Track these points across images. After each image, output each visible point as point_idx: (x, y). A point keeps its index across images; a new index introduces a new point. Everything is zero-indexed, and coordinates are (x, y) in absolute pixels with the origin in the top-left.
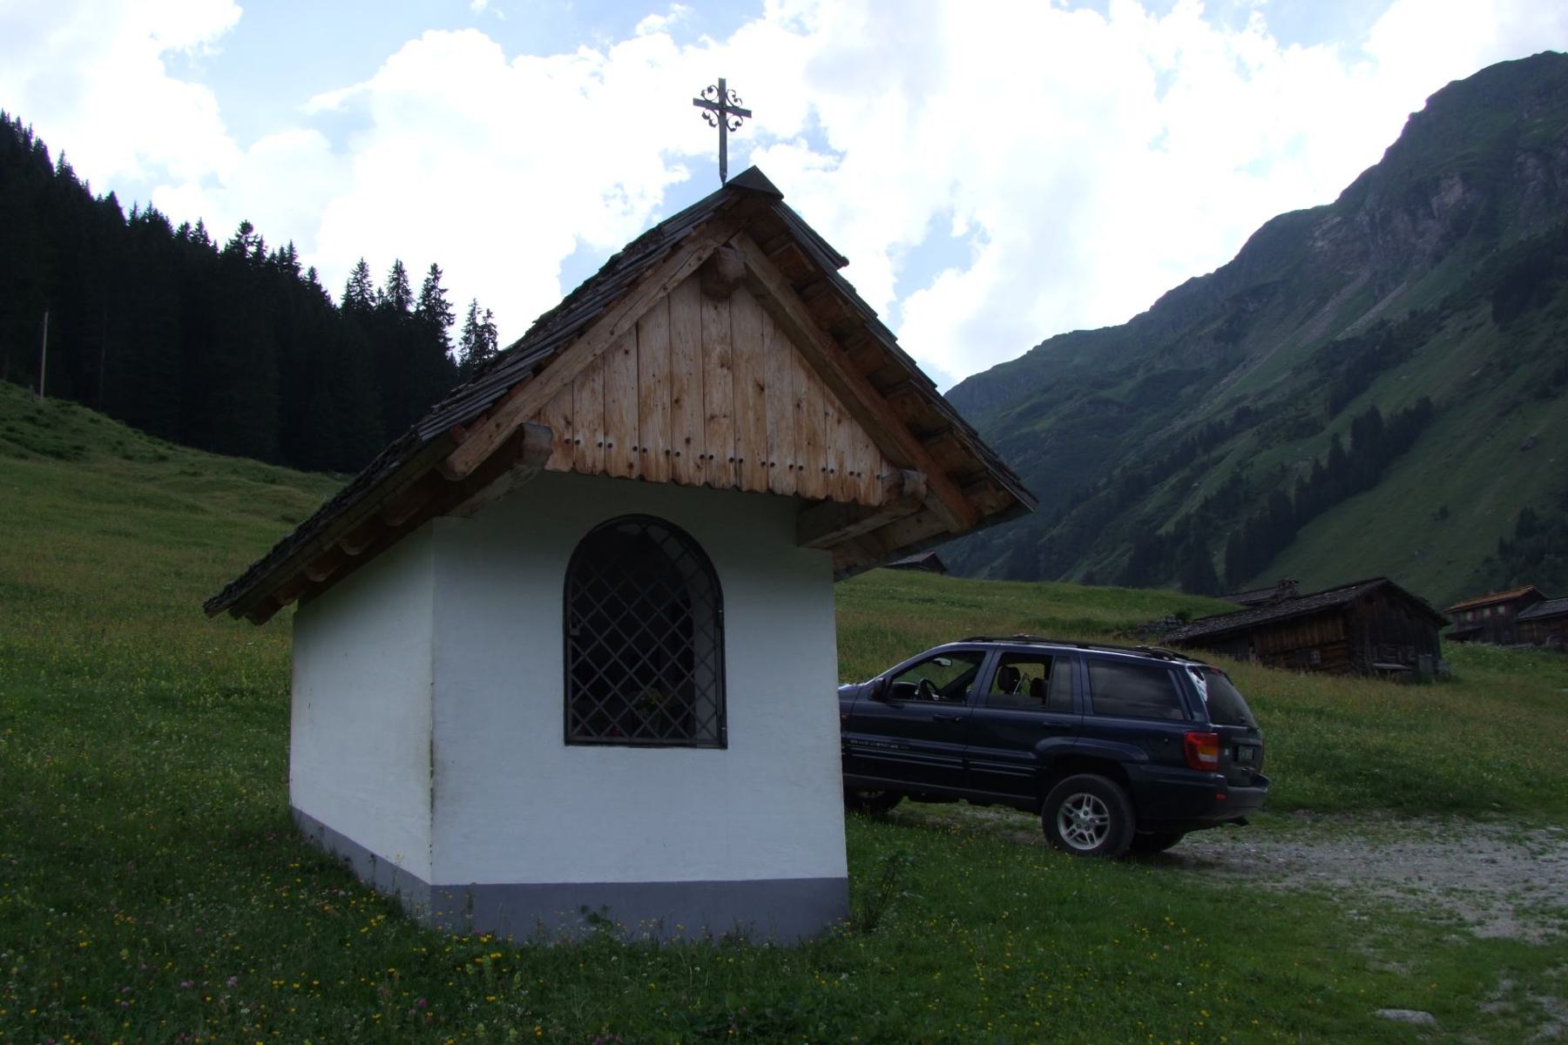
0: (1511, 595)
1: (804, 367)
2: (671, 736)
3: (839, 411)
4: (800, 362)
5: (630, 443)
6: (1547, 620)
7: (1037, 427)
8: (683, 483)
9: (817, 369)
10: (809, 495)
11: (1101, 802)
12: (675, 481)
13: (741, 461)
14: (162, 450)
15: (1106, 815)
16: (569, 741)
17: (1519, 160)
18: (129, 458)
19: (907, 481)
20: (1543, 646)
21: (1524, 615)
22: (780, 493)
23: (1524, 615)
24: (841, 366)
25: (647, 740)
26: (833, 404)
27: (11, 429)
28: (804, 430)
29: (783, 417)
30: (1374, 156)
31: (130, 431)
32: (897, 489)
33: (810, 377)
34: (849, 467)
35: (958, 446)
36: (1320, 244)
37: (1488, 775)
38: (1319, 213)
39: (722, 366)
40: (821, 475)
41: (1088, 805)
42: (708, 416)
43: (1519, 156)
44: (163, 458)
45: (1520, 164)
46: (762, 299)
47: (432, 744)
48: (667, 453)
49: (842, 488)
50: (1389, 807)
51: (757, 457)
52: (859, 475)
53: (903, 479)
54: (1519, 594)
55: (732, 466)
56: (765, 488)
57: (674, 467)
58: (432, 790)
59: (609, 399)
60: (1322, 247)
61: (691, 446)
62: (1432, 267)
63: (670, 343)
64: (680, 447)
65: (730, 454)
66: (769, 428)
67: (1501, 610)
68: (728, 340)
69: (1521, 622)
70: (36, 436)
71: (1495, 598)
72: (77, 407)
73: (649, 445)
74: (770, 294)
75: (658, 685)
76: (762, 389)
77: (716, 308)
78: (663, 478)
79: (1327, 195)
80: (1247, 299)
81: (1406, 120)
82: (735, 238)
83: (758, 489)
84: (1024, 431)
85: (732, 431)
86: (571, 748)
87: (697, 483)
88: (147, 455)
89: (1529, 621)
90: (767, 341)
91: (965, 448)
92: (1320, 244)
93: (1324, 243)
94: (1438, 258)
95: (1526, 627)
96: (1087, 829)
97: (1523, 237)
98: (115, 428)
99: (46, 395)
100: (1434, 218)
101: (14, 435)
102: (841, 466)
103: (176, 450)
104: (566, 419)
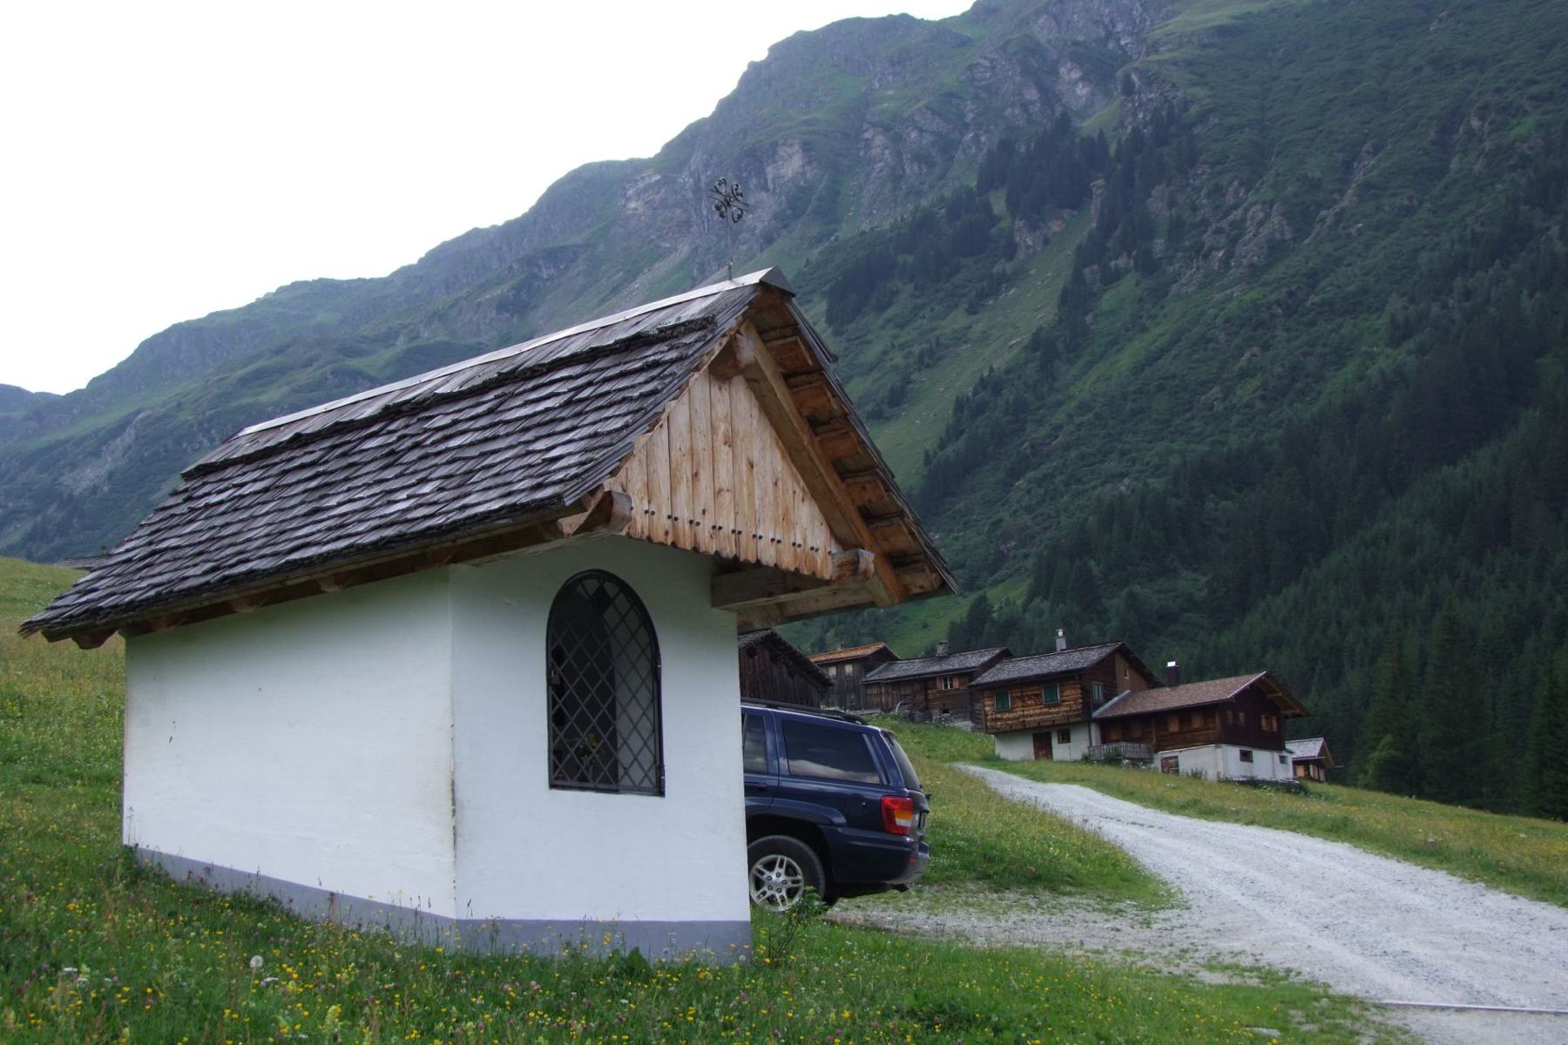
0: (860, 652)
1: (779, 448)
3: (804, 491)
4: (777, 443)
5: (666, 512)
6: (897, 683)
7: (264, 398)
9: (792, 452)
10: (784, 567)
11: (795, 864)
12: (696, 549)
13: (740, 533)
15: (800, 877)
16: (553, 786)
17: (867, 135)
19: (861, 560)
20: (892, 713)
21: (872, 676)
23: (872, 676)
25: (607, 787)
26: (799, 484)
29: (766, 492)
30: (705, 108)
32: (852, 567)
33: (783, 457)
35: (906, 531)
36: (633, 205)
38: (634, 168)
40: (792, 549)
41: (781, 866)
42: (717, 489)
43: (866, 131)
45: (867, 140)
46: (755, 383)
47: (453, 783)
48: (691, 522)
50: (978, 879)
53: (858, 557)
54: (869, 651)
58: (454, 828)
60: (636, 209)
62: (762, 250)
66: (757, 502)
67: (849, 669)
69: (868, 685)
71: (843, 655)
74: (767, 380)
75: (593, 730)
78: (689, 547)
79: (647, 145)
80: (541, 262)
81: (745, 68)
84: (245, 401)
86: (554, 791)
89: (878, 684)
90: (755, 422)
91: (911, 533)
92: (633, 205)
93: (638, 203)
94: (769, 240)
95: (875, 691)
96: (779, 890)
97: (865, 227)
100: (767, 190)
102: (805, 541)
104: (622, 486)
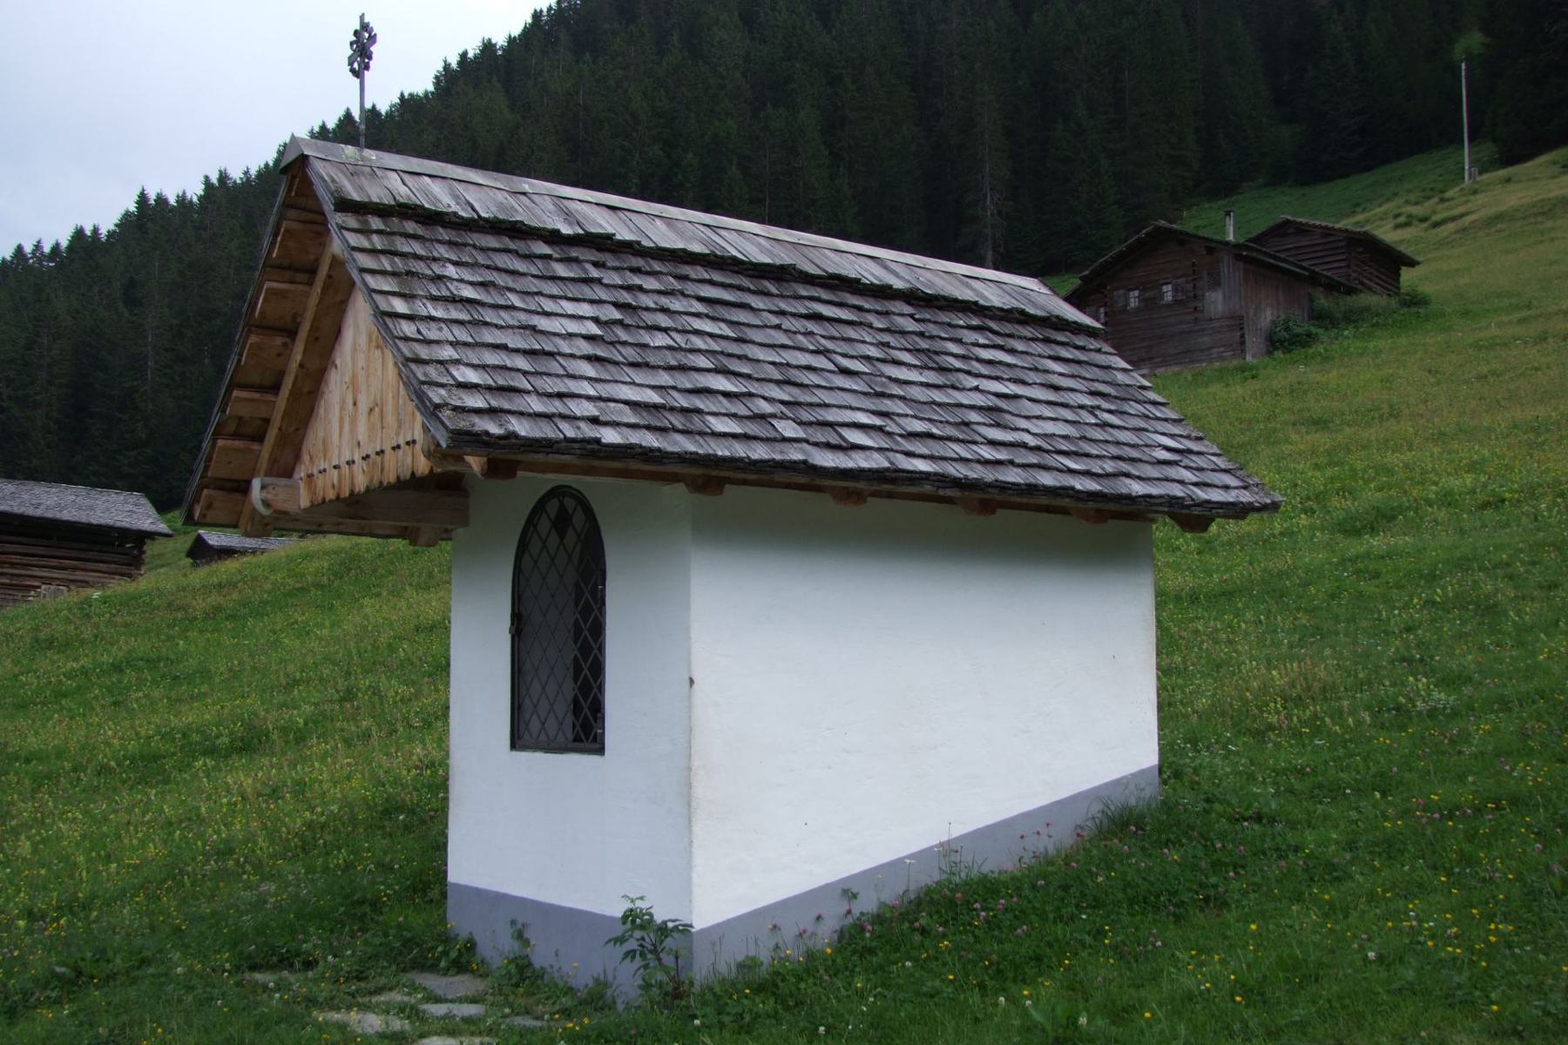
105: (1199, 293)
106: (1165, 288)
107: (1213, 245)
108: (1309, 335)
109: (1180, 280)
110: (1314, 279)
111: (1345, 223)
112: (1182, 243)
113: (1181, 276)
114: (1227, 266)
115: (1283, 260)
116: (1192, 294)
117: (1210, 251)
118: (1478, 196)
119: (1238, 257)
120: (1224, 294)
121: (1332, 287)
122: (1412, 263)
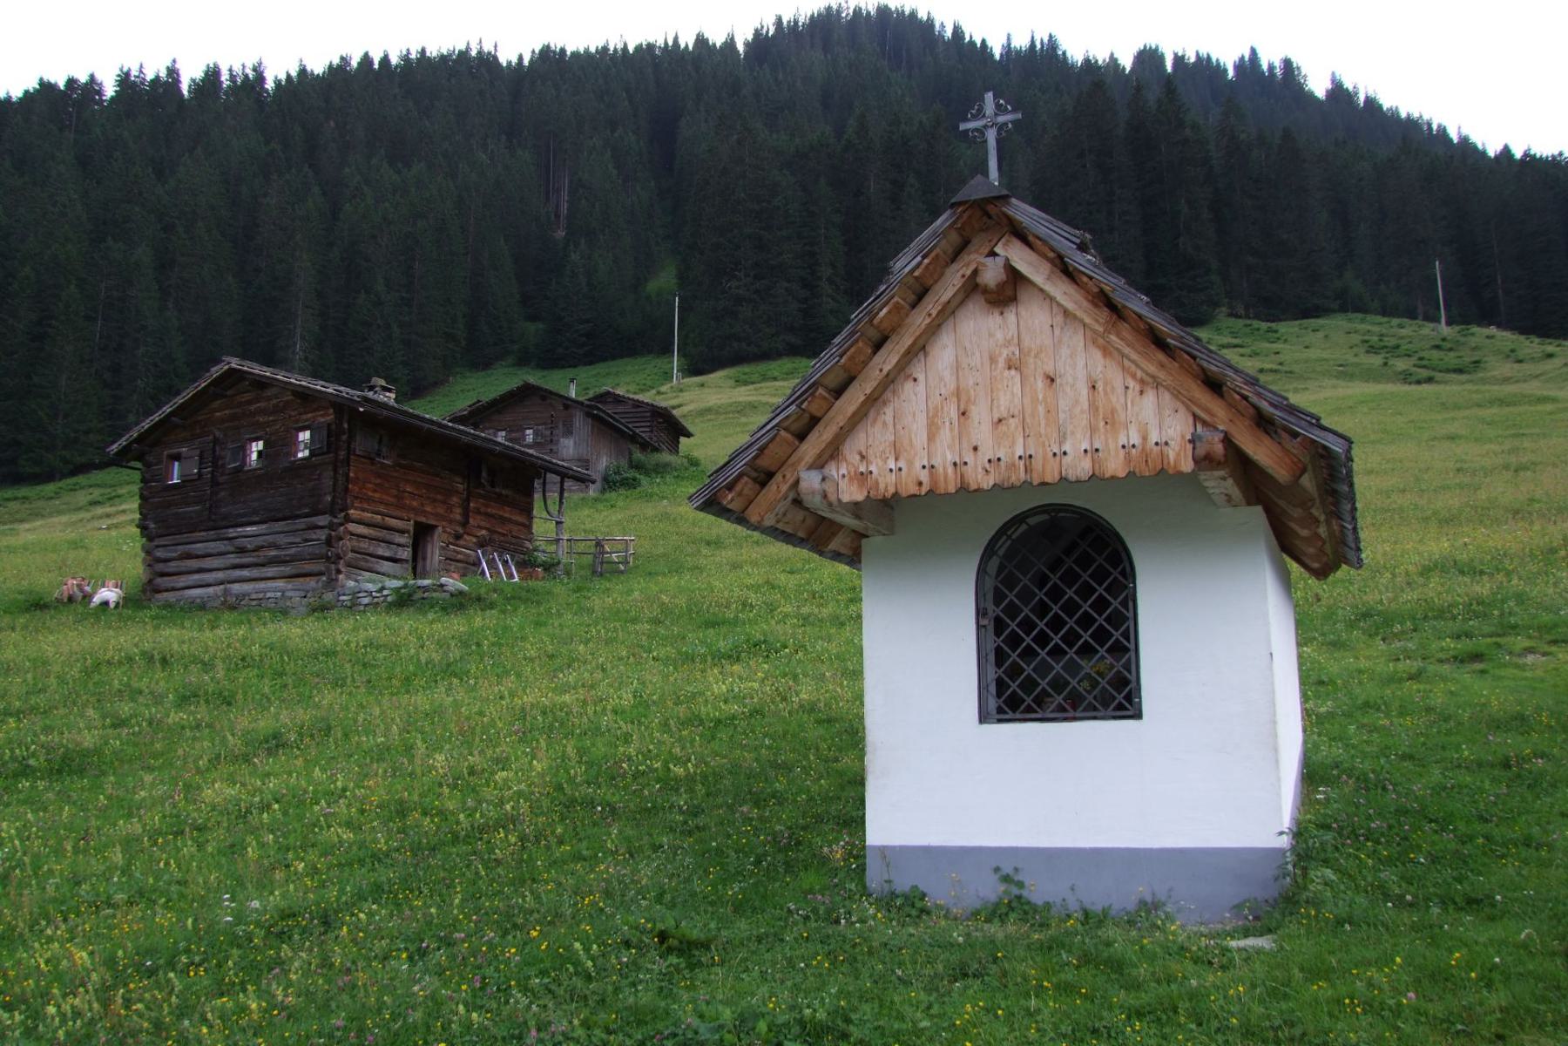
2: (1085, 710)
8: (938, 492)
14: (1550, 349)
18: (1520, 361)
22: (1074, 479)
24: (1122, 339)
27: (1421, 359)
28: (1101, 410)
29: (1077, 402)
31: (1522, 338)
34: (1154, 437)
37: (343, 981)
39: (1009, 368)
40: (1122, 452)
42: (996, 420)
44: (1550, 356)
49: (1146, 461)
51: (1049, 449)
52: (1166, 443)
55: (1022, 463)
56: (1057, 477)
57: (962, 476)
59: (899, 427)
61: (979, 453)
63: (957, 361)
64: (969, 457)
65: (1020, 452)
68: (1016, 341)
70: (1442, 360)
72: (1475, 329)
73: (937, 462)
76: (1052, 380)
77: (1002, 313)
82: (1000, 244)
83: (1049, 481)
85: (1021, 429)
87: (985, 487)
88: (1535, 355)
98: (1505, 338)
99: (1449, 323)
101: (1424, 363)
102: (1145, 439)
103: (1564, 346)
105: (555, 438)
106: (528, 432)
107: (569, 403)
108: (634, 479)
109: (540, 427)
110: (633, 438)
111: (646, 397)
112: (544, 398)
113: (542, 424)
114: (579, 420)
115: (617, 421)
116: (549, 439)
117: (566, 407)
118: (685, 394)
119: (588, 415)
120: (575, 443)
121: (645, 446)
122: (689, 435)
